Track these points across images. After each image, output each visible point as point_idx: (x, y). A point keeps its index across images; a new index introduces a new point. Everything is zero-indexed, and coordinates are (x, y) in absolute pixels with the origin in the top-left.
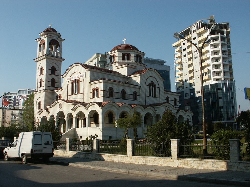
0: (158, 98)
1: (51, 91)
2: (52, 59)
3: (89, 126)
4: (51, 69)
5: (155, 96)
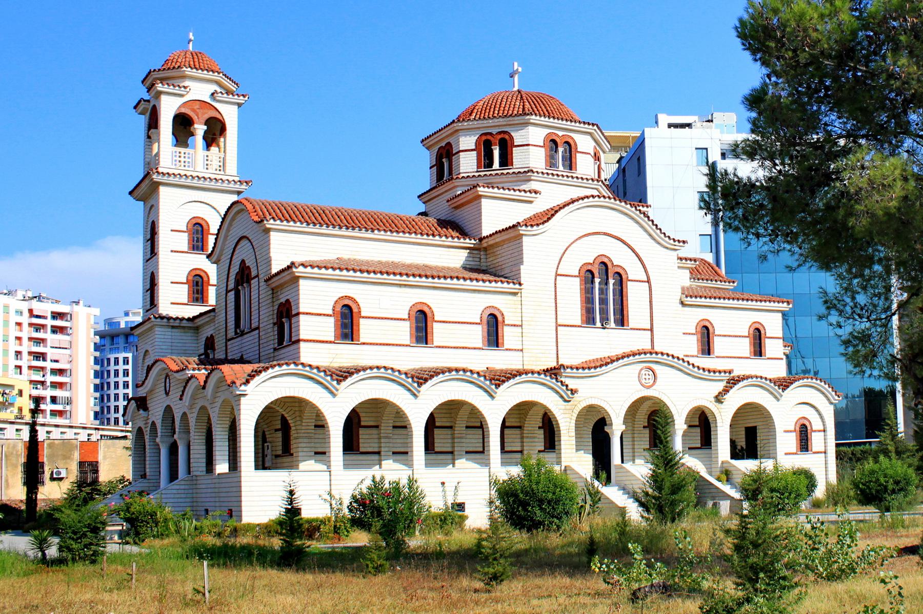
5: (622, 321)
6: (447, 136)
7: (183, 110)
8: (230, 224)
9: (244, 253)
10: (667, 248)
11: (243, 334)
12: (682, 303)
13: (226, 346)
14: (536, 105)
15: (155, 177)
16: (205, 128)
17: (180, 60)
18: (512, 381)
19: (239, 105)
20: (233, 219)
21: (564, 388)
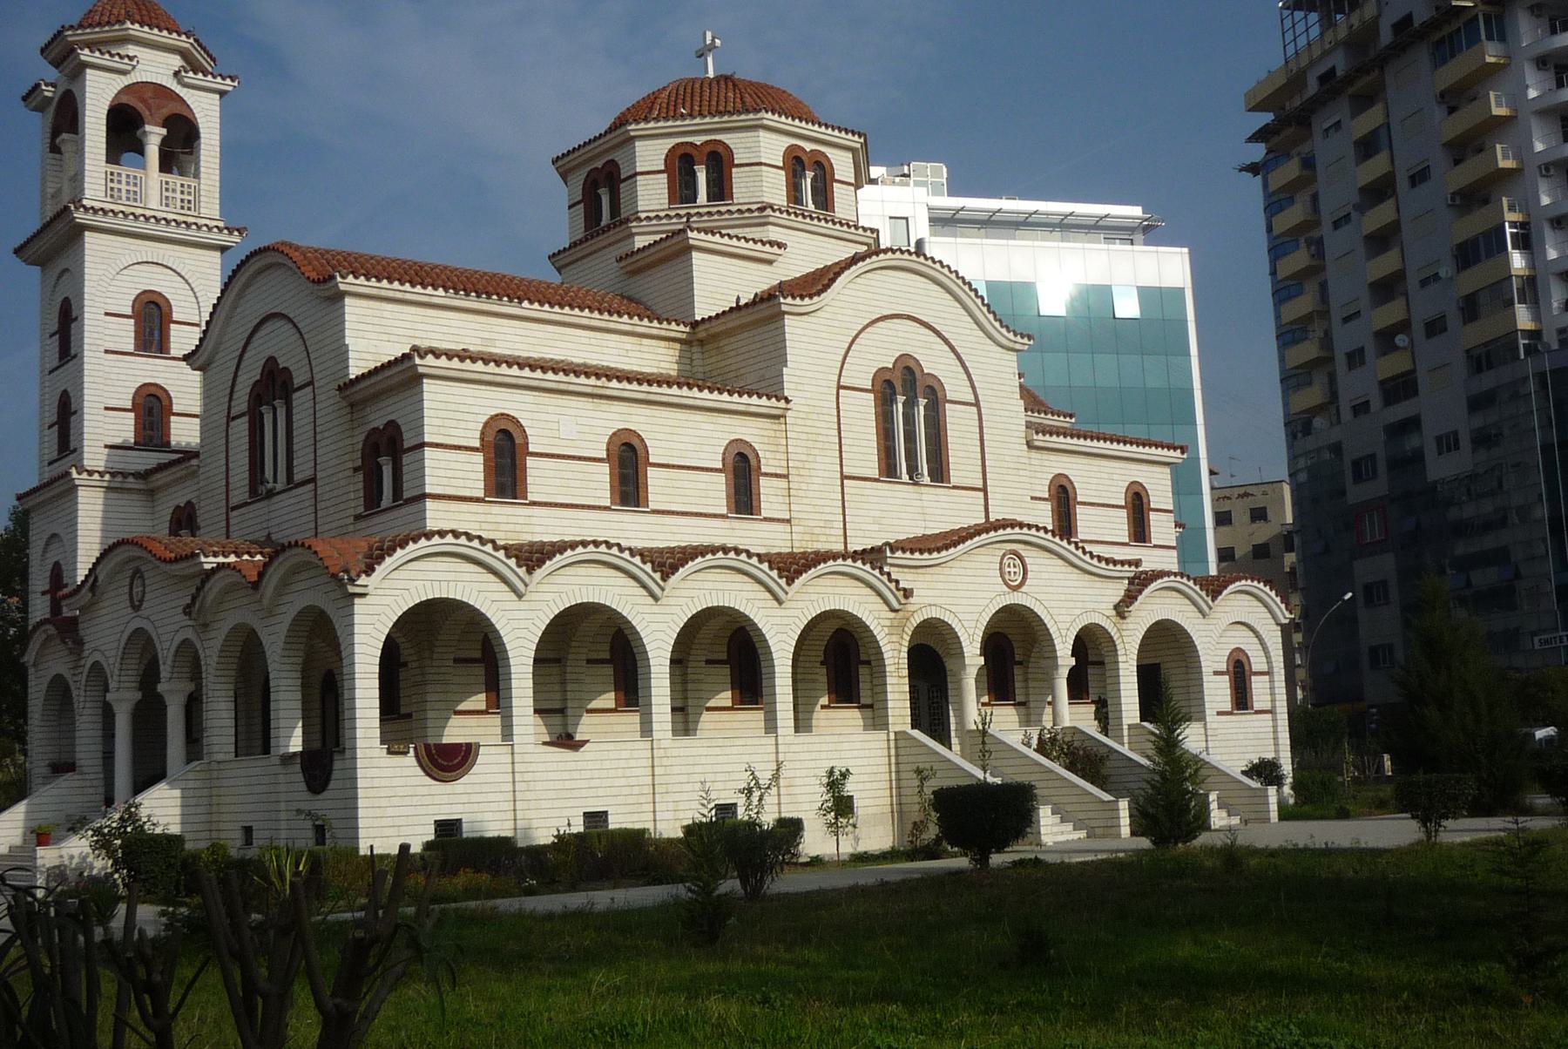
3: (802, 724)
4: (129, 311)
5: (939, 473)
6: (607, 151)
7: (124, 99)
8: (240, 295)
9: (277, 344)
10: (1002, 346)
11: (271, 494)
12: (1030, 445)
13: (227, 520)
14: (743, 97)
15: (80, 217)
16: (164, 131)
17: (115, 11)
18: (812, 572)
19: (222, 93)
20: (247, 285)
21: (892, 586)
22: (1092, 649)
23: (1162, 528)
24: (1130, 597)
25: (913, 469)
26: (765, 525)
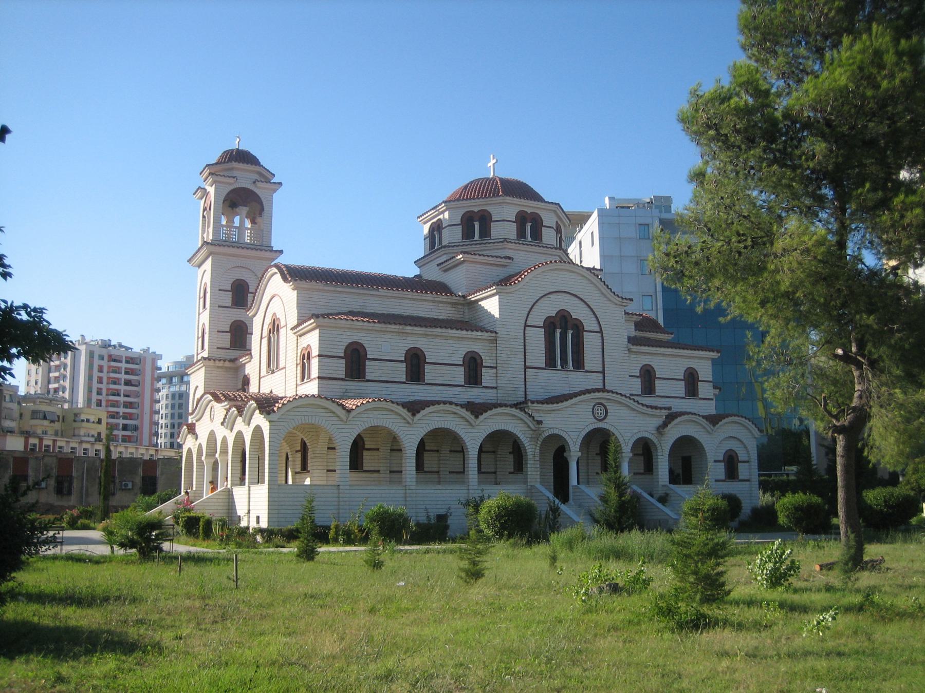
0: (335, 360)
1: (227, 364)
2: (234, 256)
5: (579, 364)
22: (645, 450)
23: (705, 390)
24: (665, 425)
25: (564, 362)
26: (484, 390)
